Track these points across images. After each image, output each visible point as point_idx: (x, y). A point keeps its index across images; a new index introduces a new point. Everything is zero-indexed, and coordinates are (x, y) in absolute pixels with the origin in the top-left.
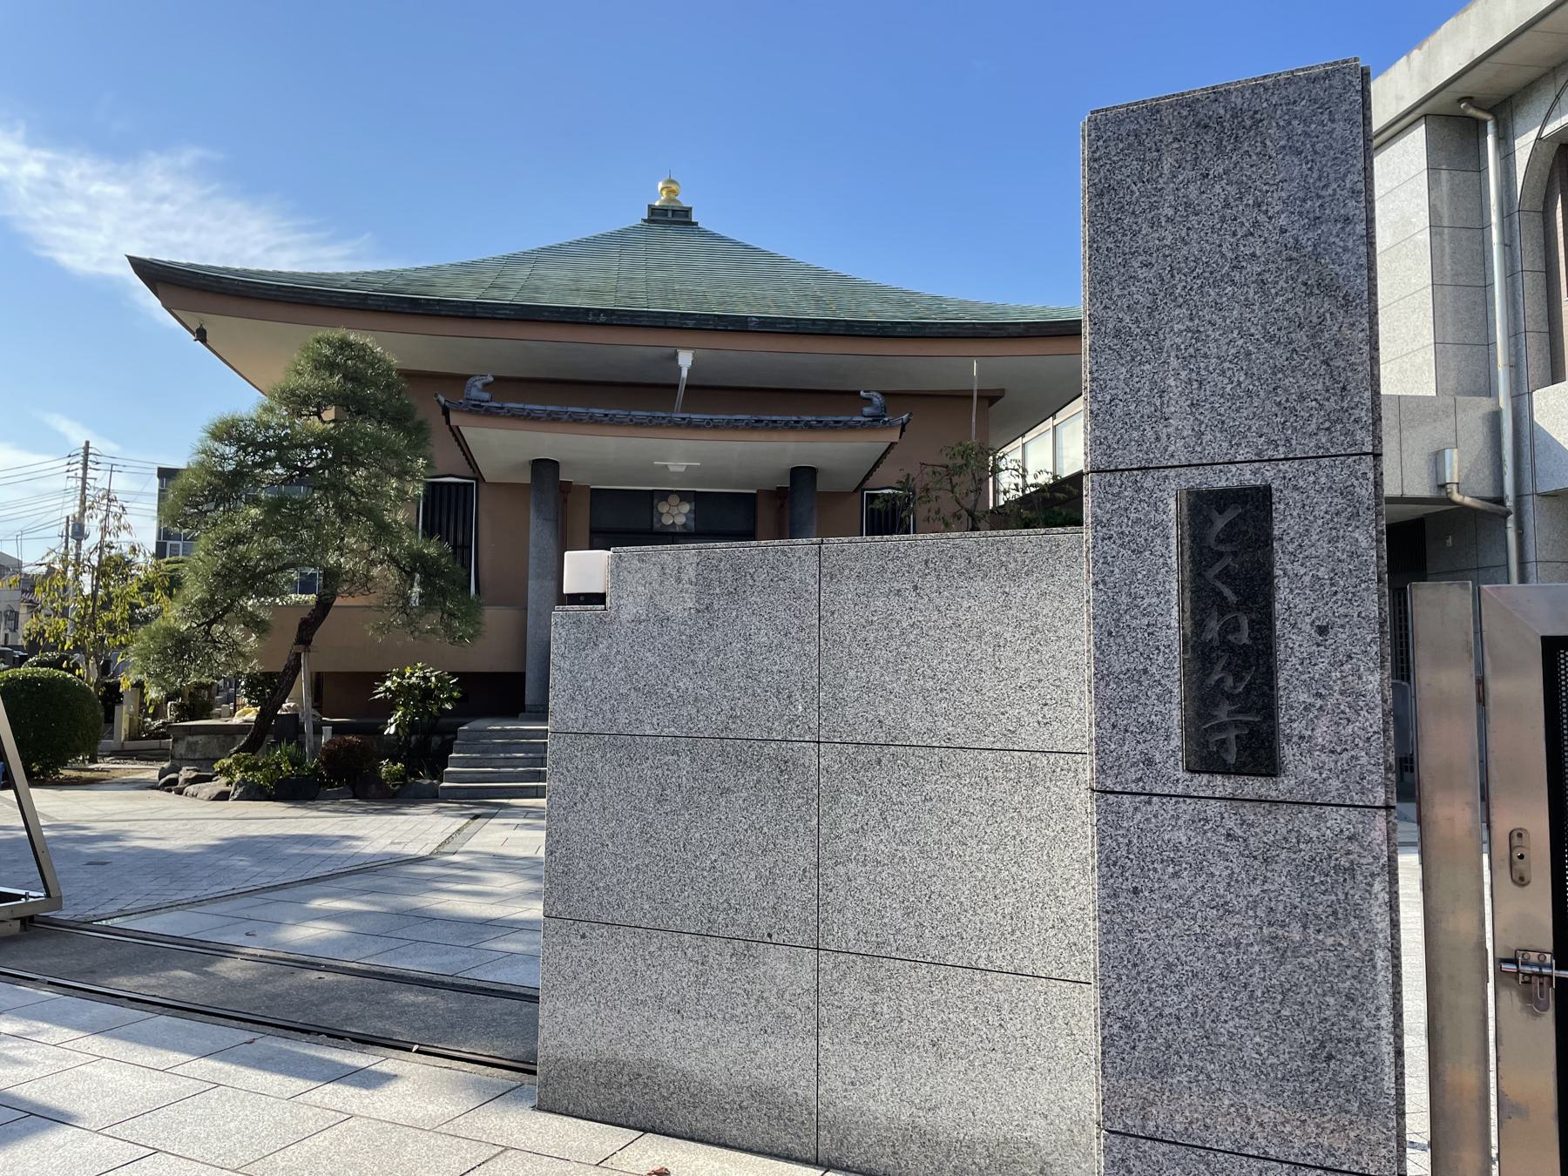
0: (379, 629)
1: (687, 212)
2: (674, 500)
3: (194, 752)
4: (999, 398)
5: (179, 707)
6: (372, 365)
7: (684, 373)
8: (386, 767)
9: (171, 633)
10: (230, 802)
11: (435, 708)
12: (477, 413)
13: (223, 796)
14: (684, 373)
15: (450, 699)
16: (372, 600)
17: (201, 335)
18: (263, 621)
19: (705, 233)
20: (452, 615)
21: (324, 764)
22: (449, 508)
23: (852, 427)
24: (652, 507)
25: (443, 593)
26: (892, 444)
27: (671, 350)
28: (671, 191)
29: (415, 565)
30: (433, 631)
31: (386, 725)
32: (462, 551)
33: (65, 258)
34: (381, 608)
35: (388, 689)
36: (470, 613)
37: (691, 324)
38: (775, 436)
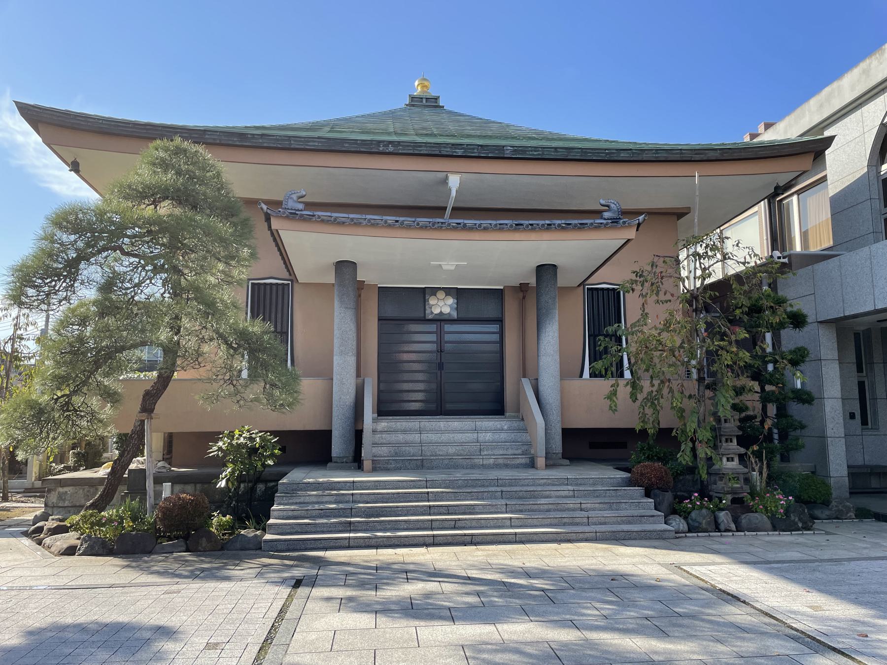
0: (207, 399)
1: (436, 99)
2: (441, 295)
3: (64, 500)
4: (687, 214)
5: (77, 455)
6: (203, 169)
7: (454, 193)
8: (218, 520)
9: (32, 405)
10: (76, 558)
11: (259, 464)
12: (293, 219)
13: (70, 551)
14: (454, 193)
15: (272, 456)
16: (202, 373)
17: (75, 167)
18: (115, 393)
19: (450, 113)
20: (273, 385)
21: (161, 520)
22: (271, 301)
23: (598, 227)
24: (425, 301)
25: (265, 366)
26: (629, 240)
27: (441, 175)
28: (424, 86)
29: (244, 342)
30: (257, 400)
31: (217, 477)
32: (283, 332)
33: (56, 187)
34: (210, 380)
35: (220, 449)
36: (290, 384)
37: (460, 152)
38: (533, 236)
